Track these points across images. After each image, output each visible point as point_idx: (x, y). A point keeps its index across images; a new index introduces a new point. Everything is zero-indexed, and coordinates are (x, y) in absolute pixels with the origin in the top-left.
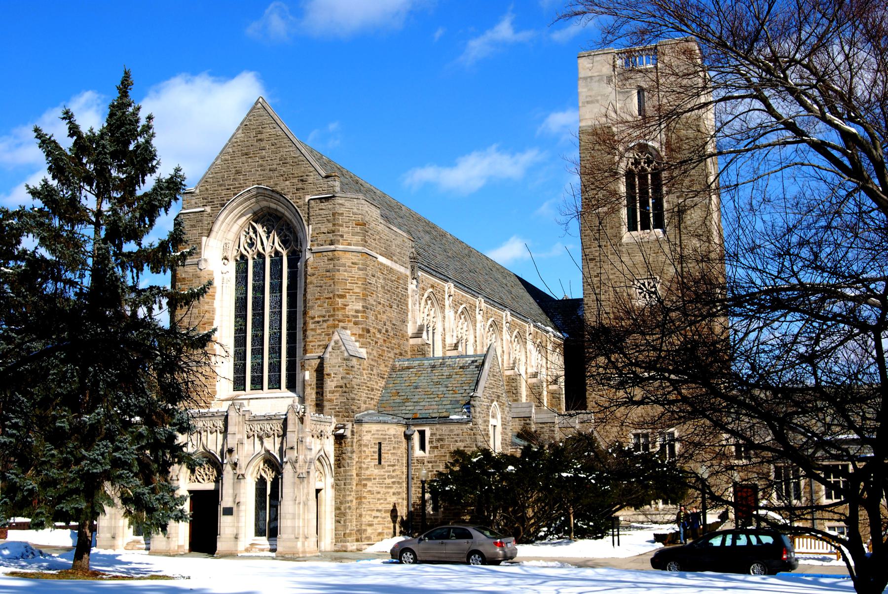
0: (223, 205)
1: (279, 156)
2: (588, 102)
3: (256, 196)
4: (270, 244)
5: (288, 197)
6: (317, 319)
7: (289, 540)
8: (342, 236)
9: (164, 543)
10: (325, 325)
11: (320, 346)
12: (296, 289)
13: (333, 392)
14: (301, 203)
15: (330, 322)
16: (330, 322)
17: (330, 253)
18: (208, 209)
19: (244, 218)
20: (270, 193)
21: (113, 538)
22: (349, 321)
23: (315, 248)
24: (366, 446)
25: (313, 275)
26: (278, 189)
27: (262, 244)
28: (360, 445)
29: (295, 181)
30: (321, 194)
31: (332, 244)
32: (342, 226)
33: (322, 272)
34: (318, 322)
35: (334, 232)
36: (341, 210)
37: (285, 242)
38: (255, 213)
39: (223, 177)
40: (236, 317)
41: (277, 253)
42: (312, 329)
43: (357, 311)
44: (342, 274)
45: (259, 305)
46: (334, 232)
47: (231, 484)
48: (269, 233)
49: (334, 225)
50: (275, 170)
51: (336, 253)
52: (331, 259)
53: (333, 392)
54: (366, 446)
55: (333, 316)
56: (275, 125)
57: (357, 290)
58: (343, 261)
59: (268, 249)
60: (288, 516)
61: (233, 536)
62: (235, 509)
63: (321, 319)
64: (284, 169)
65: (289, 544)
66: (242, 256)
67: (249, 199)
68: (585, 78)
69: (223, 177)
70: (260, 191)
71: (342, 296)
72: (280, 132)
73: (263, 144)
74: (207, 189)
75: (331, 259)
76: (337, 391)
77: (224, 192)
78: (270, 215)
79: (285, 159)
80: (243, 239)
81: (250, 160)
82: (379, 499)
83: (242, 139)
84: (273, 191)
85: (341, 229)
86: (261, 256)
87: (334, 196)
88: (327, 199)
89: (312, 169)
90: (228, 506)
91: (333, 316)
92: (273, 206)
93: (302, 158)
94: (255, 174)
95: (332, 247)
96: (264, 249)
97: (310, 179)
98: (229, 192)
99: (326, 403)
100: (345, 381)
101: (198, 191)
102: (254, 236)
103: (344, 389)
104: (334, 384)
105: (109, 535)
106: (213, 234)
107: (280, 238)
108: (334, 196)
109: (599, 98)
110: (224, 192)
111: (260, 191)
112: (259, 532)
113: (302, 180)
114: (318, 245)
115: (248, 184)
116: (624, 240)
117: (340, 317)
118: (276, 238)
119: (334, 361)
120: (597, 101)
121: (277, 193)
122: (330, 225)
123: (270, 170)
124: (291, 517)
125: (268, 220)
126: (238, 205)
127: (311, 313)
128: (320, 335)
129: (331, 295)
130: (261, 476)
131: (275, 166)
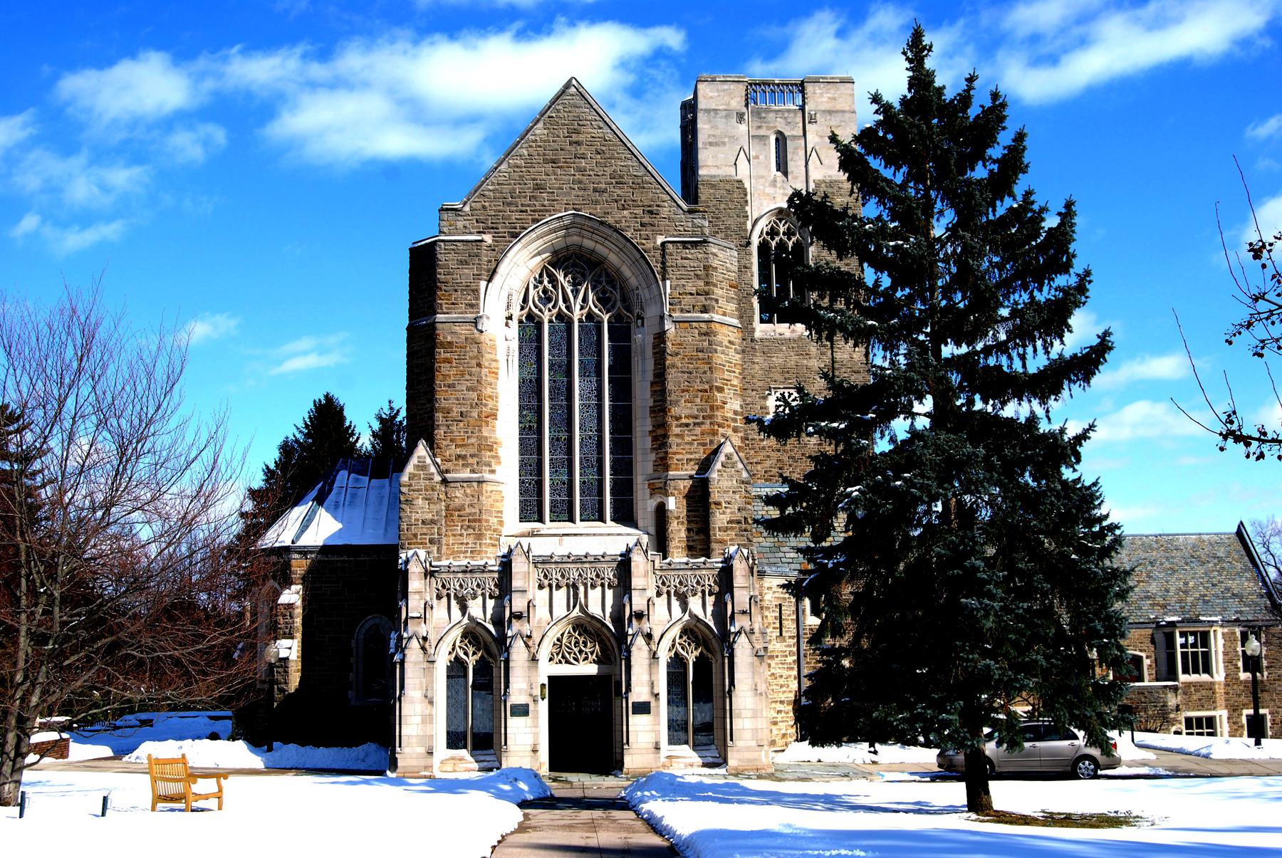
0: (515, 235)
1: (609, 170)
2: (711, 144)
3: (567, 228)
4: (581, 304)
5: (629, 235)
6: (684, 421)
7: (748, 749)
8: (717, 301)
9: (529, 759)
10: (698, 430)
11: (689, 460)
12: (630, 373)
13: (726, 529)
14: (649, 245)
15: (707, 427)
16: (707, 427)
17: (703, 325)
18: (488, 238)
19: (539, 259)
20: (596, 225)
21: (431, 753)
22: (729, 426)
23: (676, 315)
24: (768, 608)
25: (677, 354)
26: (610, 220)
27: (566, 300)
28: (762, 608)
29: (639, 211)
30: (679, 236)
31: (705, 310)
32: (715, 286)
33: (690, 351)
34: (687, 425)
35: (707, 294)
36: (715, 263)
37: (603, 301)
38: (555, 253)
39: (512, 192)
40: (521, 408)
41: (590, 316)
42: (677, 435)
43: (736, 413)
44: (719, 358)
45: (564, 392)
46: (707, 294)
47: (646, 667)
48: (576, 285)
49: (707, 284)
50: (605, 191)
51: (713, 325)
52: (706, 334)
53: (726, 529)
54: (768, 608)
55: (710, 417)
56: (602, 124)
57: (735, 382)
58: (720, 337)
59: (577, 314)
60: (744, 713)
61: (652, 746)
62: (653, 705)
63: (691, 421)
64: (619, 192)
65: (748, 755)
66: (530, 317)
67: (560, 229)
68: (708, 111)
69: (512, 192)
70: (578, 220)
71: (720, 390)
72: (610, 136)
73: (581, 150)
74: (484, 207)
75: (706, 334)
76: (732, 528)
77: (515, 216)
78: (580, 257)
79: (621, 177)
80: (532, 292)
81: (559, 171)
82: (782, 686)
83: (544, 138)
84: (602, 223)
85: (716, 290)
86: (564, 320)
87: (705, 241)
88: (695, 244)
89: (666, 197)
90: (642, 699)
91: (710, 417)
92: (588, 244)
93: (648, 178)
94: (569, 194)
95: (706, 316)
96: (568, 308)
97: (665, 212)
98: (524, 216)
99: (714, 545)
100: (744, 514)
101: (467, 208)
102: (550, 287)
103: (744, 526)
104: (726, 517)
105: (422, 750)
106: (498, 279)
107: (596, 294)
108: (705, 241)
109: (726, 140)
110: (515, 216)
111: (578, 220)
112: (455, 740)
113: (651, 212)
114: (682, 311)
115: (557, 207)
116: (757, 335)
117: (720, 420)
118: (591, 295)
119: (725, 484)
120: (724, 144)
121: (610, 226)
122: (701, 283)
123: (595, 190)
124: (749, 714)
125: (574, 265)
126: (538, 238)
127: (675, 411)
128: (691, 444)
129: (707, 387)
130: (457, 658)
131: (603, 186)
